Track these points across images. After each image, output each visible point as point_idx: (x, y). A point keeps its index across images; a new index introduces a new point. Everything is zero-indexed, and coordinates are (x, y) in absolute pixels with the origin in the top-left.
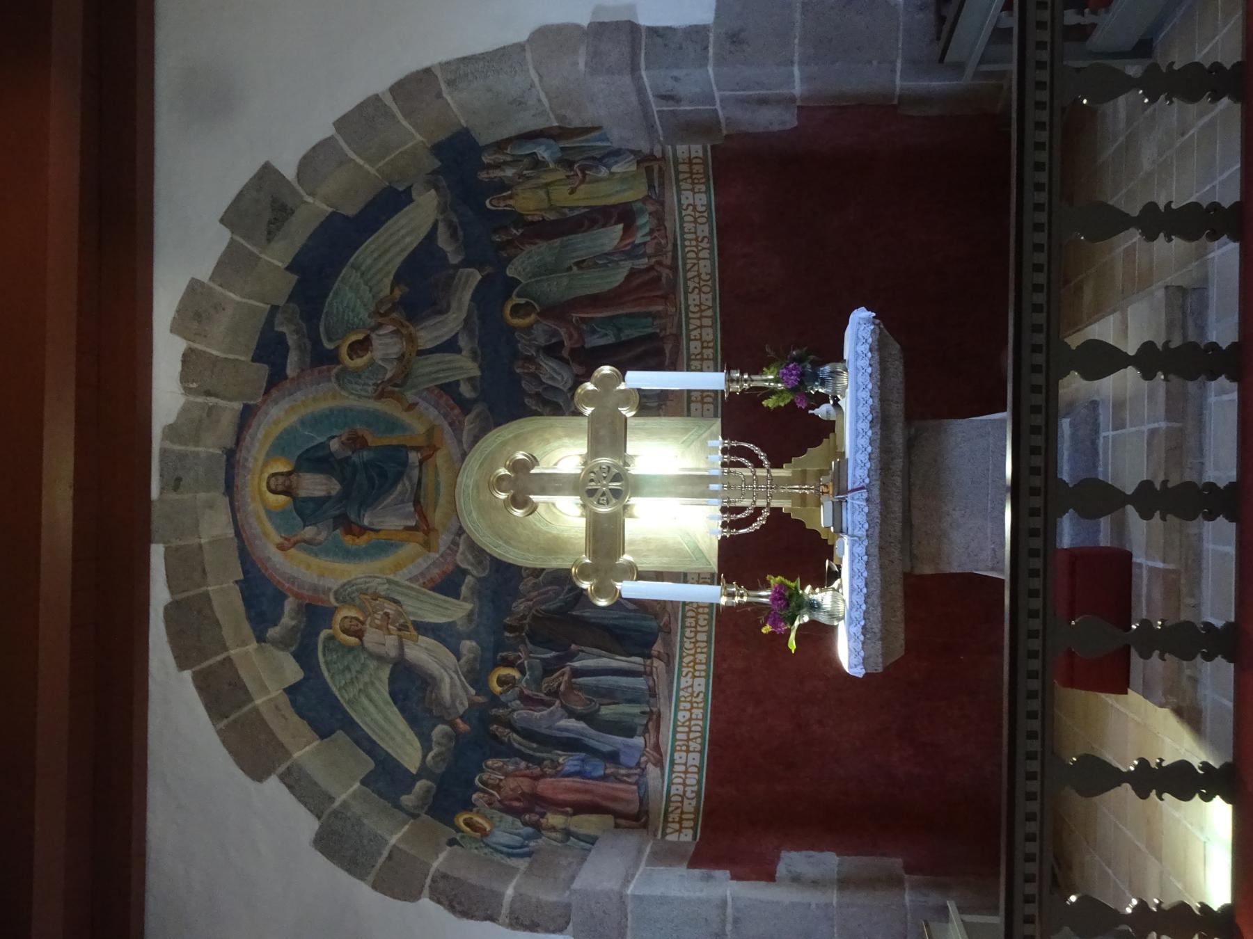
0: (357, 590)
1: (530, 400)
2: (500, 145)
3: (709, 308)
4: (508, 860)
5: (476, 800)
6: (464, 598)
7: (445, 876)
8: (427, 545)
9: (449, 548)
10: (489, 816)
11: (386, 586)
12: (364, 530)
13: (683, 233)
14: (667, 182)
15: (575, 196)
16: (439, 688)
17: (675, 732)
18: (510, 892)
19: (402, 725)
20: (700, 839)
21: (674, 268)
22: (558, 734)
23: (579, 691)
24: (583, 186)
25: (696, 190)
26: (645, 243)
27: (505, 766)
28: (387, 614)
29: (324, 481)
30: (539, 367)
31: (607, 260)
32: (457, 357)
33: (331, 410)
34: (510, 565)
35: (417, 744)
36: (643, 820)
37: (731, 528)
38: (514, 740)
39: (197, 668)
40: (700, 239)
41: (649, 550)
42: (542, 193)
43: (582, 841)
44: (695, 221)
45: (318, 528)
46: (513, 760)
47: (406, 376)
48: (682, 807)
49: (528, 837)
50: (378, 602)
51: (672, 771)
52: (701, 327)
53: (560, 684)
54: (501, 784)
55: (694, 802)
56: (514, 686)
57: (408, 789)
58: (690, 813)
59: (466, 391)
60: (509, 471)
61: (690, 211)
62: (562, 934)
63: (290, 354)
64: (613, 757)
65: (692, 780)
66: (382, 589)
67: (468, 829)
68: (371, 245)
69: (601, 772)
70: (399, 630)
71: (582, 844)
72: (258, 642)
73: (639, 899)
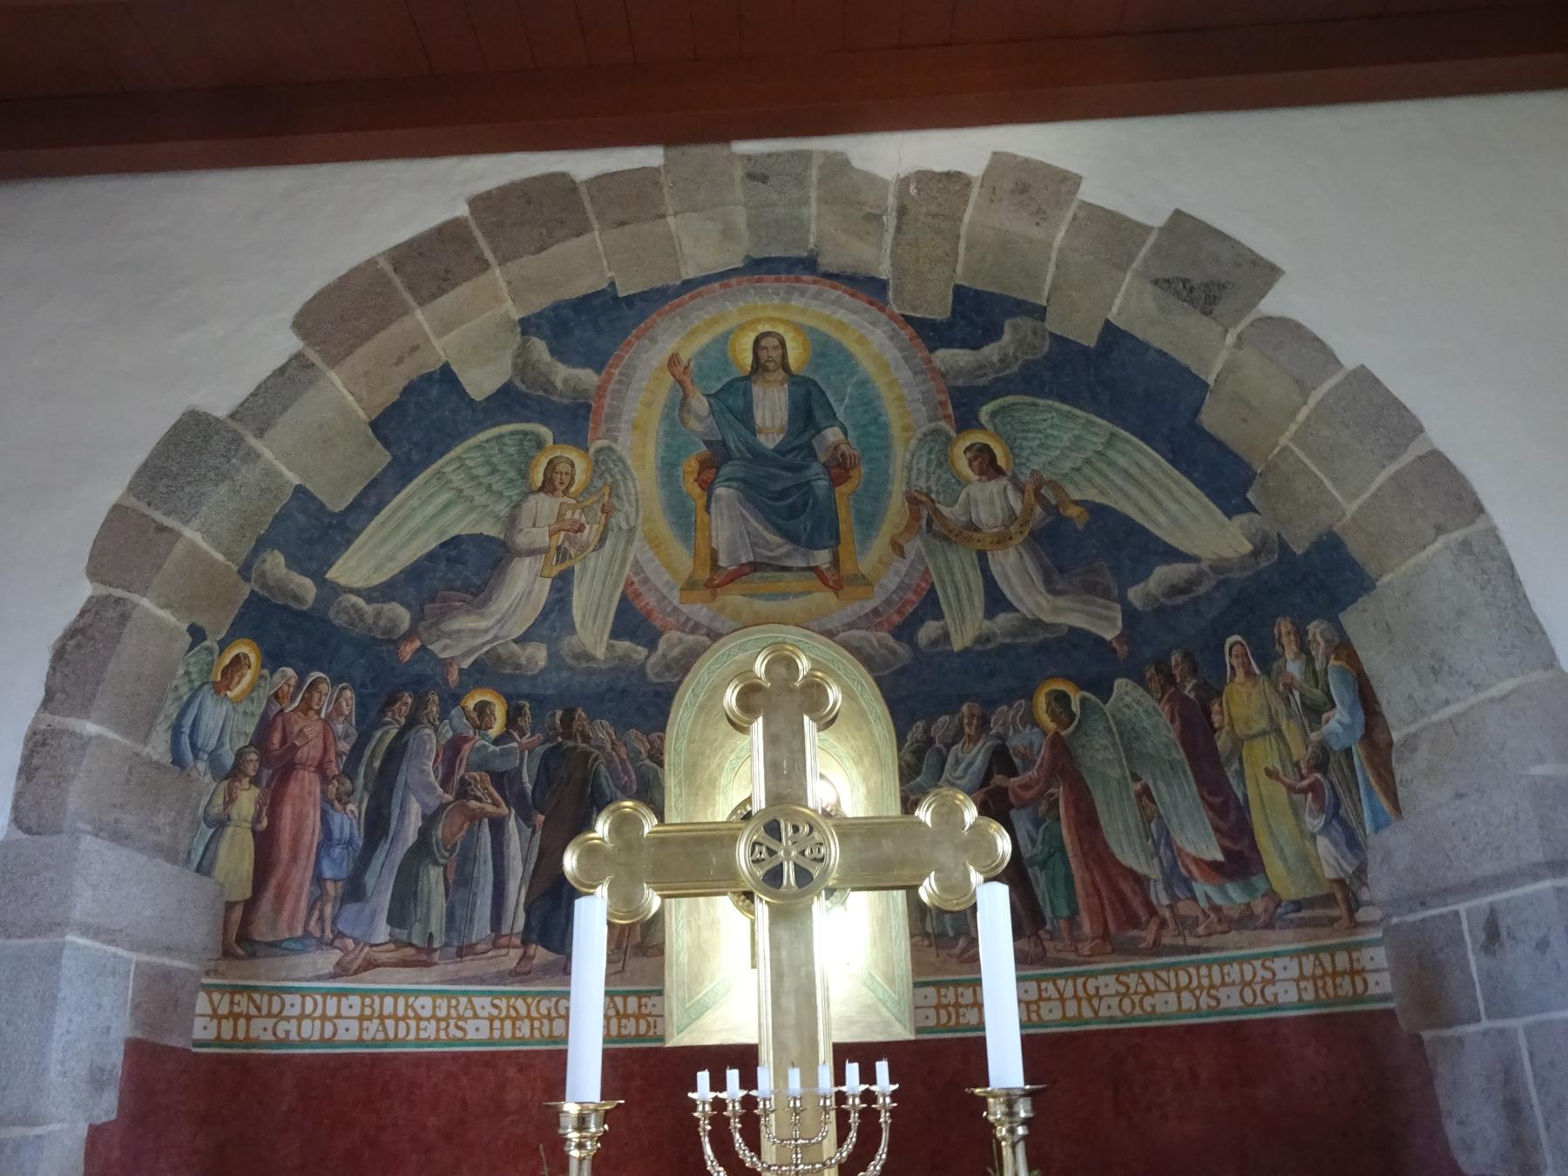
0: (616, 482)
1: (920, 730)
2: (1343, 648)
3: (1096, 1012)
4: (165, 726)
5: (284, 675)
6: (612, 646)
7: (124, 618)
8: (690, 585)
9: (688, 619)
10: (255, 694)
11: (624, 526)
12: (707, 487)
13: (1222, 963)
14: (1310, 931)
15: (1263, 778)
16: (468, 612)
17: (396, 994)
18: (91, 728)
19: (410, 554)
20: (197, 1054)
21: (1156, 949)
22: (396, 801)
23: (468, 831)
24: (1284, 790)
25: (1302, 984)
26: (1194, 898)
27: (342, 719)
28: (581, 529)
29: (778, 423)
30: (973, 740)
31: (1160, 838)
32: (980, 614)
33: (885, 426)
34: (665, 715)
35: (377, 580)
36: (240, 951)
37: (712, 1120)
38: (387, 732)
39: (472, 224)
40: (1213, 992)
41: (699, 928)
42: (1263, 724)
43: (207, 848)
44: (1246, 983)
45: (706, 418)
46: (353, 731)
47: (946, 539)
48: (260, 1016)
49: (214, 760)
50: (600, 514)
51: (326, 993)
52: (1062, 999)
53: (478, 799)
54: (311, 713)
55: (268, 1036)
56: (477, 728)
57: (294, 563)
58: (247, 1031)
59: (928, 631)
60: (804, 677)
61: (1261, 973)
62: (11, 822)
63: (968, 352)
64: (355, 891)
65: (310, 1030)
66: (619, 520)
67: (227, 661)
68: (1150, 460)
69: (328, 873)
70: (558, 548)
71: (201, 850)
72: (522, 321)
73: (54, 959)
